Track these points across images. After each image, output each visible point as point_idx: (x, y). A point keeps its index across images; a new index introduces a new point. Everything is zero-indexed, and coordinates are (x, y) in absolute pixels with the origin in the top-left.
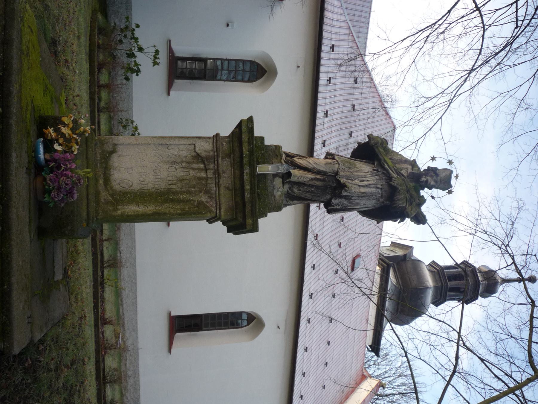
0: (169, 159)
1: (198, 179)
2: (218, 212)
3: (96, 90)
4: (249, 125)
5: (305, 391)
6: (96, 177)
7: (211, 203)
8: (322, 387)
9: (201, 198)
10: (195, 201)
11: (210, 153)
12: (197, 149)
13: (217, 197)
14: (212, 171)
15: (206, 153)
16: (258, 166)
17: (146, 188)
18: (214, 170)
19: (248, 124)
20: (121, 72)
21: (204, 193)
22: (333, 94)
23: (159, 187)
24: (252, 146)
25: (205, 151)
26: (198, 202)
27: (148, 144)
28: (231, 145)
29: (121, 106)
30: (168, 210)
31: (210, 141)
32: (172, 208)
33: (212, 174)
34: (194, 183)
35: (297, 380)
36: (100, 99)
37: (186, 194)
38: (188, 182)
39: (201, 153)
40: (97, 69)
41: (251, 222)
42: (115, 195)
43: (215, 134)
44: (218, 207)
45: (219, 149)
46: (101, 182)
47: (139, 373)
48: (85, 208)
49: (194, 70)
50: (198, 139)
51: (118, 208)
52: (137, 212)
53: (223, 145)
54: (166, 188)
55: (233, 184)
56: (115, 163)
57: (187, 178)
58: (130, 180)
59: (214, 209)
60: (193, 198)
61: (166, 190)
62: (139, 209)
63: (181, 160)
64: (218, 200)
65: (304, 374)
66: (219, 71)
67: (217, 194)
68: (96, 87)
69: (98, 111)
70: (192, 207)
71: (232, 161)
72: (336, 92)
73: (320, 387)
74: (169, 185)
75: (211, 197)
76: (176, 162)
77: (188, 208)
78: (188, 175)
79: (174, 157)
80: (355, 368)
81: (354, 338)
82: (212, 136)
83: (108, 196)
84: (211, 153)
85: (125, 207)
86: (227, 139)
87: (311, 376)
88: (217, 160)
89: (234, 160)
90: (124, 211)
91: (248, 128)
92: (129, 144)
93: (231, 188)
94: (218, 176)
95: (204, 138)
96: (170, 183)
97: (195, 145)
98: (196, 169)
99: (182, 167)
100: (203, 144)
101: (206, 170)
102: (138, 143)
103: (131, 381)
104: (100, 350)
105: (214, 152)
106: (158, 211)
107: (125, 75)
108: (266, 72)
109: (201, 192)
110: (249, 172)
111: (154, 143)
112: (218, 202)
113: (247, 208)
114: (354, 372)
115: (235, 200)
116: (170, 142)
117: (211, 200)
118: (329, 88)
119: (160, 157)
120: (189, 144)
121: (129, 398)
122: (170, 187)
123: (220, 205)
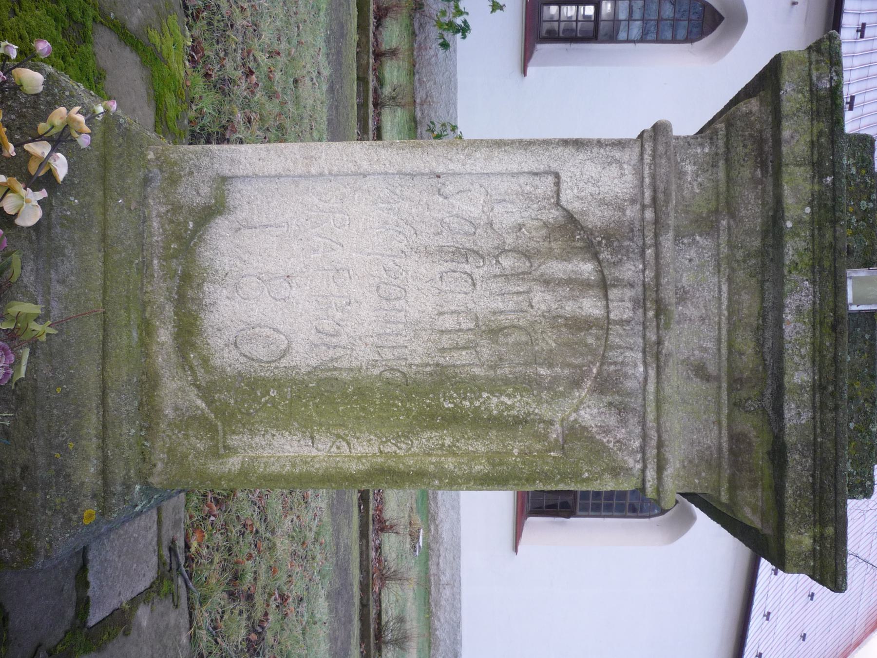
0: (445, 240)
1: (566, 325)
2: (651, 474)
3: (372, 61)
4: (819, 78)
5: (767, 646)
6: (147, 315)
7: (621, 434)
8: (799, 637)
9: (576, 410)
10: (551, 423)
11: (623, 210)
12: (567, 196)
13: (651, 409)
14: (629, 293)
15: (608, 213)
16: (850, 273)
17: (345, 364)
18: (640, 289)
19: (815, 74)
20: (433, 32)
21: (592, 391)
22: (866, 60)
23: (399, 358)
24: (829, 179)
25: (602, 202)
26: (562, 426)
27: (355, 174)
28: (722, 175)
29: (434, 99)
30: (434, 460)
31: (626, 158)
32: (451, 452)
33: (629, 305)
34: (549, 341)
35: (754, 626)
36: (380, 81)
37: (516, 390)
38: (524, 338)
39: (583, 213)
40: (375, 18)
41: (807, 541)
42: (220, 392)
43: (648, 126)
44: (652, 452)
45: (667, 193)
46: (164, 335)
47: (460, 581)
48: (92, 445)
49: (574, 24)
50: (569, 151)
51: (229, 442)
52: (306, 463)
53: (681, 174)
54: (427, 365)
55: (724, 351)
56: (223, 255)
57: (522, 322)
58: (281, 327)
59: (631, 462)
60: (544, 411)
61: (431, 374)
62: (314, 452)
63: (496, 242)
64: (651, 423)
65: (768, 616)
66: (623, 23)
67: (651, 397)
68: (371, 55)
69: (376, 105)
70: (538, 446)
71: (725, 250)
72: (873, 55)
73: (796, 635)
74: (443, 350)
75: (622, 410)
76: (477, 253)
77: (522, 454)
78: (525, 306)
79: (467, 228)
80: (865, 603)
81: (869, 547)
82: (634, 136)
83: (193, 393)
84: (628, 212)
85: (257, 439)
86: (702, 145)
87: (779, 619)
88: (657, 245)
89: (731, 246)
90: (252, 459)
91: (813, 90)
92: (279, 176)
93: (712, 369)
94: (657, 316)
95: (600, 143)
96: (446, 342)
97: (557, 176)
98: (560, 283)
99: (498, 271)
100: (592, 169)
101: (604, 286)
102: (313, 171)
103: (447, 593)
104: (371, 582)
105: (644, 207)
106: (391, 463)
107: (442, 37)
108: (721, 18)
109: (576, 383)
110: (808, 306)
111: (382, 169)
112: (653, 434)
113: (791, 474)
114: (863, 610)
115: (730, 427)
116: (451, 166)
117: (623, 422)
118: (861, 46)
119: (408, 230)
120: (536, 174)
121: (442, 620)
122: (445, 360)
123: (660, 445)
